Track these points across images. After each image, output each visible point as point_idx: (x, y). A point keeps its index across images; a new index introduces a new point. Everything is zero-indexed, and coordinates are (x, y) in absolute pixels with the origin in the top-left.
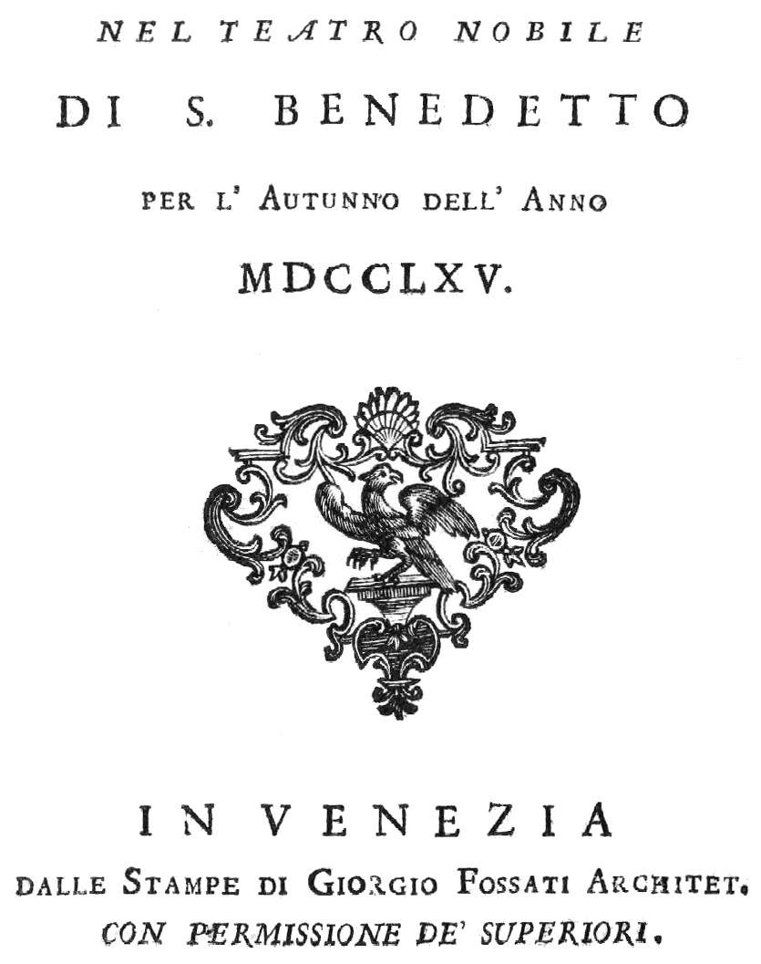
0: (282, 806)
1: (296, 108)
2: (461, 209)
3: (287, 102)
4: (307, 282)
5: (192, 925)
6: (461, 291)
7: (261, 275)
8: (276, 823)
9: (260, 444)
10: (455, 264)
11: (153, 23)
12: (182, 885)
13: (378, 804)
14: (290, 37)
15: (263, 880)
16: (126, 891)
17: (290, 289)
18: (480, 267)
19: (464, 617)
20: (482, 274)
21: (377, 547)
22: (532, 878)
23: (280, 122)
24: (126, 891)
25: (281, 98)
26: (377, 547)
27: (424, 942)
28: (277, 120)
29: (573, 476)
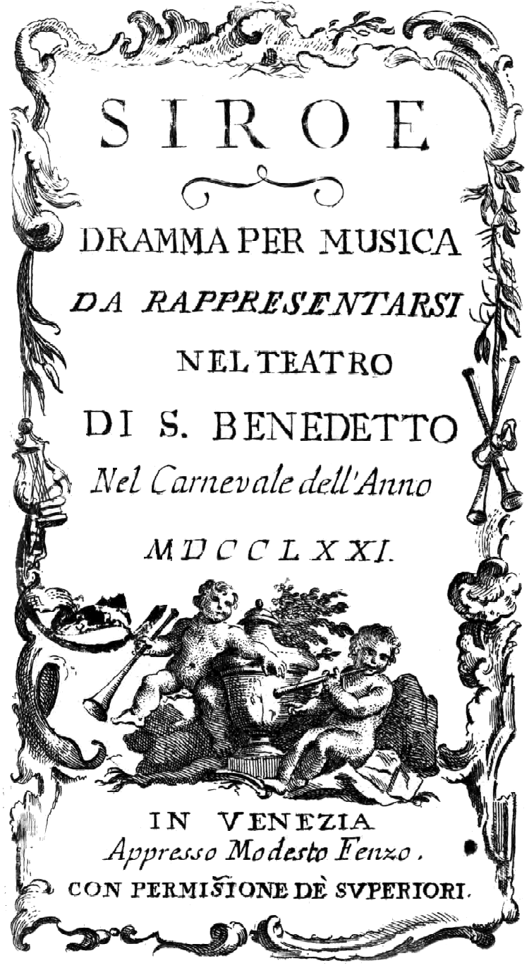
0: (285, 541)
2: (161, 896)
3: (226, 419)
5: (342, 231)
6: (318, 542)
7: (195, 236)
8: (274, 819)
9: (127, 58)
10: (362, 493)
13: (270, 412)
16: (337, 895)
17: (299, 896)
20: (222, 243)
22: (310, 354)
23: (219, 437)
24: (337, 895)
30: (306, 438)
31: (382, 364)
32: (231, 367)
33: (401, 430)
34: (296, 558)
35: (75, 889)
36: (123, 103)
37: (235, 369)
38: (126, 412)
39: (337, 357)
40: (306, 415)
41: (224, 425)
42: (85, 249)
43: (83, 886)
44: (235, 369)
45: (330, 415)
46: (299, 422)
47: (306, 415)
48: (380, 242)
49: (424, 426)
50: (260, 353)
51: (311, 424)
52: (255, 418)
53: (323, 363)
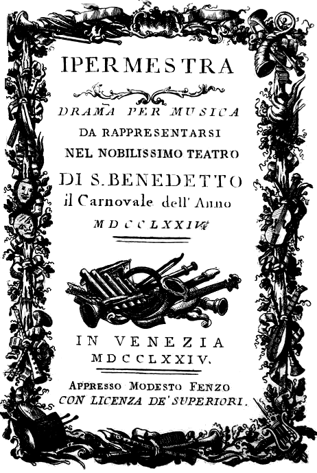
12: (198, 133)
15: (109, 355)
22: (207, 152)
23: (112, 184)
25: (104, 130)
32: (85, 155)
34: (155, 362)
36: (166, 71)
37: (220, 176)
38: (79, 337)
41: (113, 178)
42: (62, 184)
44: (220, 176)
46: (75, 152)
52: (80, 151)
53: (212, 155)
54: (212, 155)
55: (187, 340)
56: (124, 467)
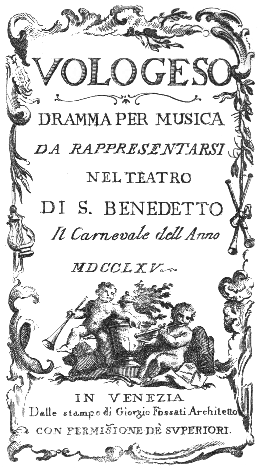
1: (106, 35)
3: (110, 205)
4: (51, 211)
11: (141, 281)
14: (38, 103)
18: (154, 182)
19: (131, 413)
21: (86, 318)
22: (151, 174)
23: (107, 214)
26: (86, 318)
27: (125, 272)
28: (148, 213)
29: (170, 452)
30: (149, 214)
31: (186, 178)
33: (195, 210)
35: (40, 431)
39: (164, 175)
40: (149, 203)
43: (43, 429)
45: (161, 203)
46: (146, 206)
47: (149, 203)
48: (185, 119)
49: (206, 208)
50: (127, 173)
51: (152, 207)
53: (158, 178)
54: (158, 178)
55: (160, 396)
56: (232, 217)
